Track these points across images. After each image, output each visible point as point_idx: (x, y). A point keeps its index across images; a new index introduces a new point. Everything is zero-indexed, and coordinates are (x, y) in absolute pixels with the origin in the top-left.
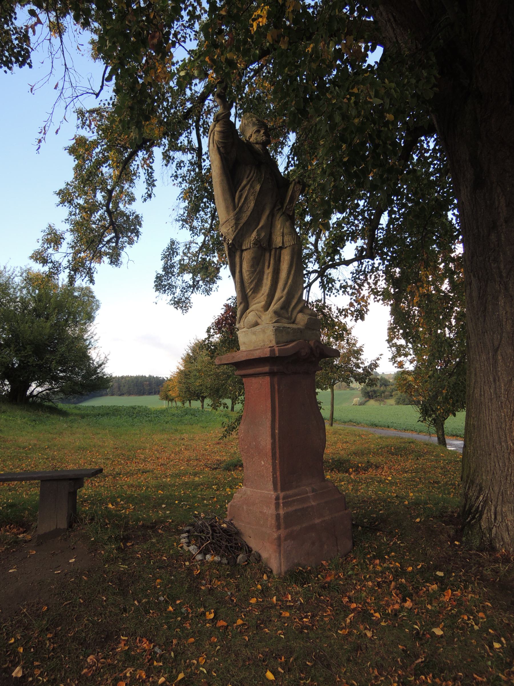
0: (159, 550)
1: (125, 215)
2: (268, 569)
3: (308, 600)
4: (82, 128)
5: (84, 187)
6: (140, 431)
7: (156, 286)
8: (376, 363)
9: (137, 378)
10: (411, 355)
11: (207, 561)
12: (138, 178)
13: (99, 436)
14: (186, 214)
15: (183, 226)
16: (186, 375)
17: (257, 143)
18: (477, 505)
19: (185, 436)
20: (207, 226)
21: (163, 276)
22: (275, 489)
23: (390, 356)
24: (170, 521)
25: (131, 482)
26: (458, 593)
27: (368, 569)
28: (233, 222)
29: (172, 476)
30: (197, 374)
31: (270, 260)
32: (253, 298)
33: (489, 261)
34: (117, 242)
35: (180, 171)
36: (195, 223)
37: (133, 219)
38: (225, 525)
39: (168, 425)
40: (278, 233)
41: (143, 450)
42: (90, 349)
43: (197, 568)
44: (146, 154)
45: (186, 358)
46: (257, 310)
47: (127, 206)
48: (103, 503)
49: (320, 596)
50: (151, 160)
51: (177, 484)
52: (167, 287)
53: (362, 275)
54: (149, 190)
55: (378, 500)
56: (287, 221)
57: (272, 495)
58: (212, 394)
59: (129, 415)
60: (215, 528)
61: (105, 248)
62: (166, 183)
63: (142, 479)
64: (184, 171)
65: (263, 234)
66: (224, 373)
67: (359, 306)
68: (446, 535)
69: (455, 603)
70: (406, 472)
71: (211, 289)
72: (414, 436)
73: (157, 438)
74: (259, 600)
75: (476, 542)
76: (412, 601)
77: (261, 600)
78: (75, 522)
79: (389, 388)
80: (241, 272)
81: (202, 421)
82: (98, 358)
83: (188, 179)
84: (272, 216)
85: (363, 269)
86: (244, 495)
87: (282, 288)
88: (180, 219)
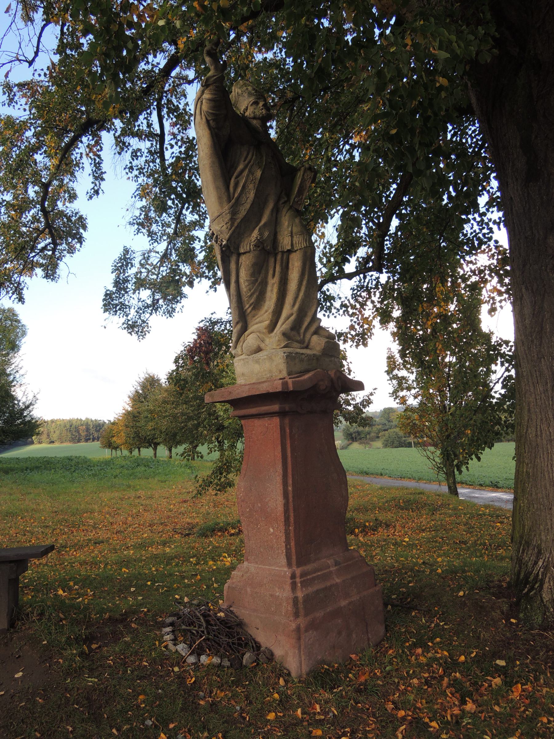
0: (136, 653)
1: (66, 216)
2: (285, 671)
3: (342, 710)
4: (9, 105)
5: (13, 179)
6: (83, 488)
7: (105, 305)
8: (369, 399)
9: (70, 421)
10: (415, 388)
11: (202, 665)
12: (81, 170)
13: (32, 496)
14: (142, 216)
15: (138, 231)
16: (134, 417)
17: (254, 118)
18: (535, 572)
19: (141, 493)
20: (170, 231)
21: (114, 293)
22: (289, 565)
23: (391, 390)
24: (146, 610)
25: (83, 557)
26: (529, 687)
27: (409, 661)
28: (229, 217)
29: (135, 547)
30: (149, 416)
31: (275, 267)
32: (254, 317)
33: (546, 270)
34: (54, 250)
35: (135, 163)
36: (154, 227)
37: (75, 221)
38: (222, 614)
39: (116, 481)
40: (286, 233)
41: (91, 513)
42: (14, 386)
43: (190, 674)
44: (93, 140)
45: (134, 396)
46: (260, 332)
47: (67, 204)
48: (50, 589)
49: (356, 703)
50: (99, 147)
51: (144, 558)
52: (118, 307)
53: (363, 292)
54: (96, 185)
55: (403, 568)
56: (296, 217)
57: (285, 572)
58: (167, 440)
59: (65, 469)
60: (210, 619)
61: (37, 257)
62: (119, 177)
63: (96, 552)
64: (141, 161)
65: (266, 234)
66: (183, 414)
67: (361, 329)
68: (498, 611)
69: (527, 701)
70: (423, 531)
71: (174, 310)
72: (423, 486)
73: (106, 496)
74: (279, 714)
75: (538, 619)
76: (473, 701)
77: (281, 715)
78: (18, 619)
79: (375, 429)
80: (237, 282)
81: (159, 473)
82: (25, 397)
83: (147, 172)
84: (276, 211)
85: (366, 284)
86: (246, 572)
87: (292, 303)
88: (135, 222)
